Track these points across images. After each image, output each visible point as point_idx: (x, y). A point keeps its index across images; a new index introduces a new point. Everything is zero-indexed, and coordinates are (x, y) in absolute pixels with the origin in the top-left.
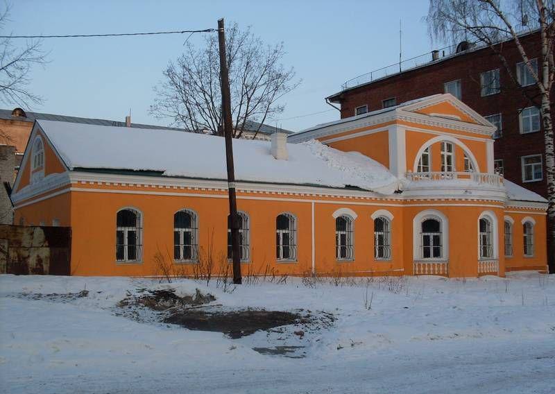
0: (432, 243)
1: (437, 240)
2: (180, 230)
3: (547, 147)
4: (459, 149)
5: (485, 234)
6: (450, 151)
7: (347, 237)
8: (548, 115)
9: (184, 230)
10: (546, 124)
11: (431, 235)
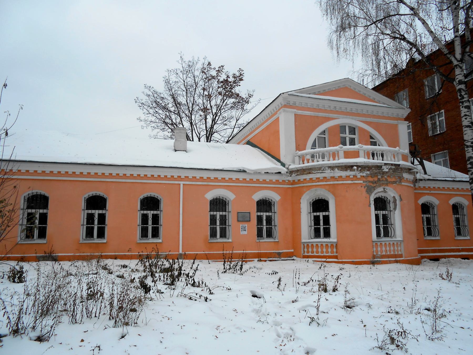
0: (150, 222)
1: (327, 220)
2: (149, 212)
3: (463, 119)
4: (362, 130)
8: (463, 86)
9: (152, 212)
10: (461, 95)
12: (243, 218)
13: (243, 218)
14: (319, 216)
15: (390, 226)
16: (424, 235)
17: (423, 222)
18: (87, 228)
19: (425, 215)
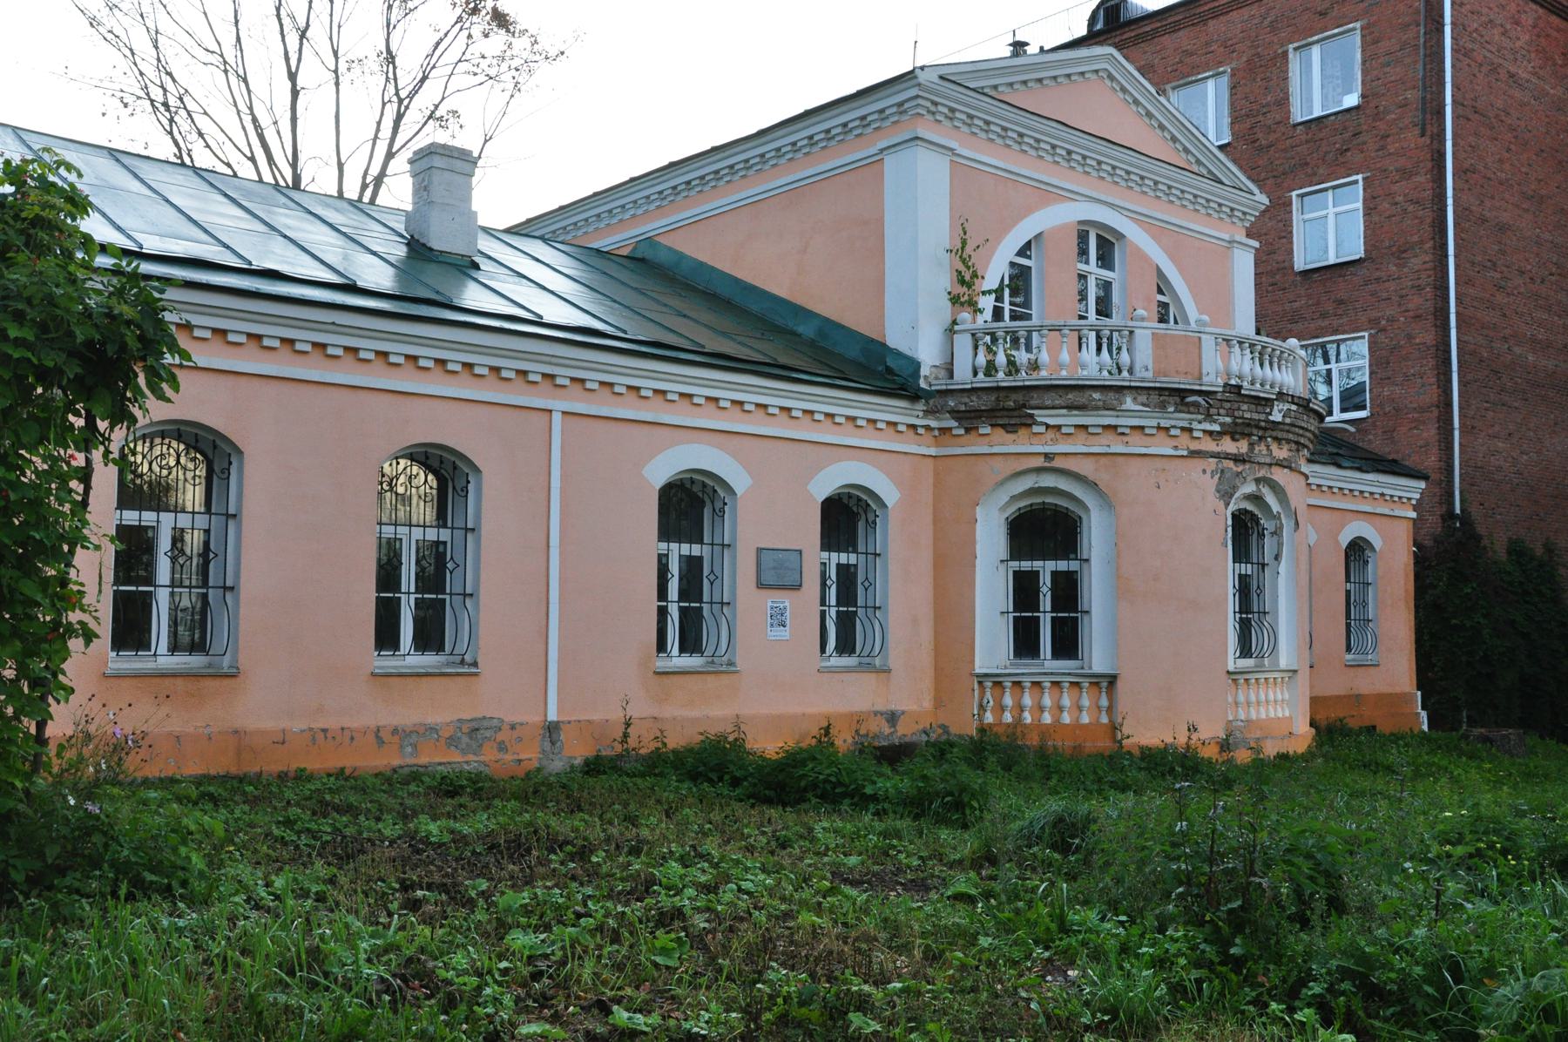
0: (1046, 602)
1: (1068, 591)
5: (1247, 569)
6: (1105, 260)
7: (706, 572)
9: (1051, 565)
11: (1046, 569)
12: (777, 574)
13: (777, 574)
14: (1034, 575)
15: (458, 600)
16: (823, 650)
17: (824, 585)
18: (117, 595)
19: (834, 555)
